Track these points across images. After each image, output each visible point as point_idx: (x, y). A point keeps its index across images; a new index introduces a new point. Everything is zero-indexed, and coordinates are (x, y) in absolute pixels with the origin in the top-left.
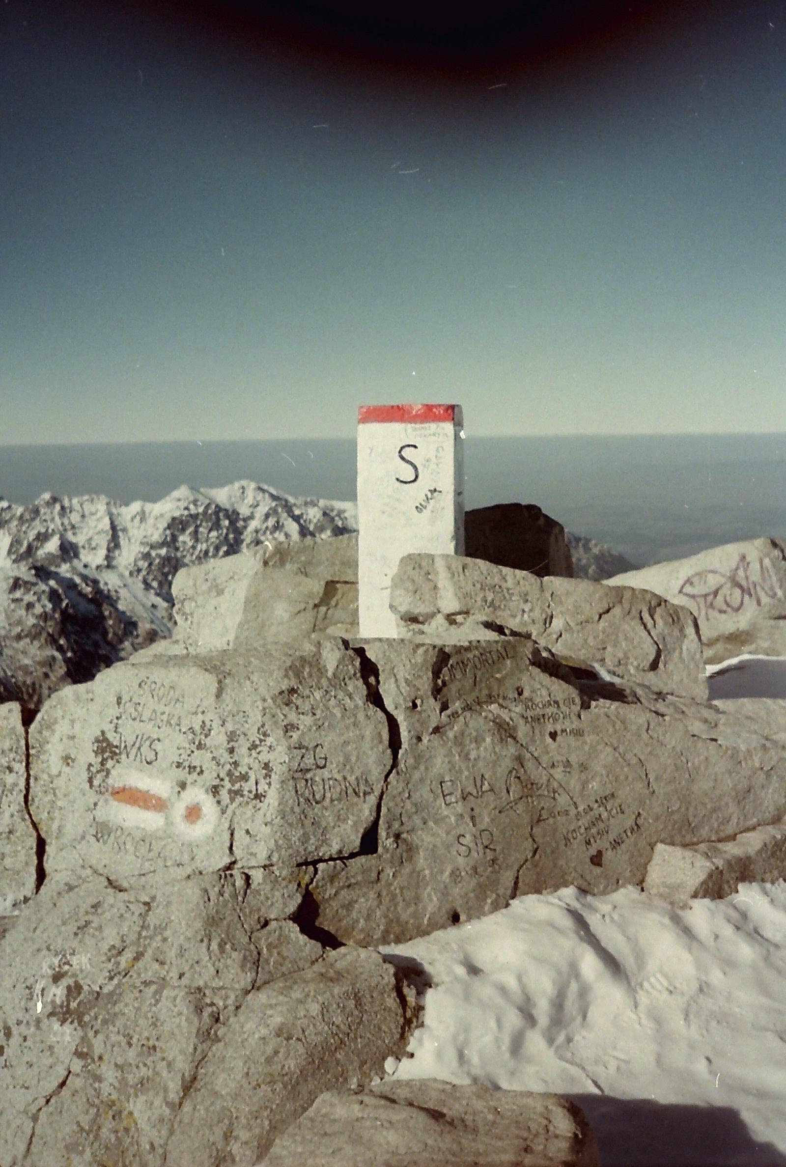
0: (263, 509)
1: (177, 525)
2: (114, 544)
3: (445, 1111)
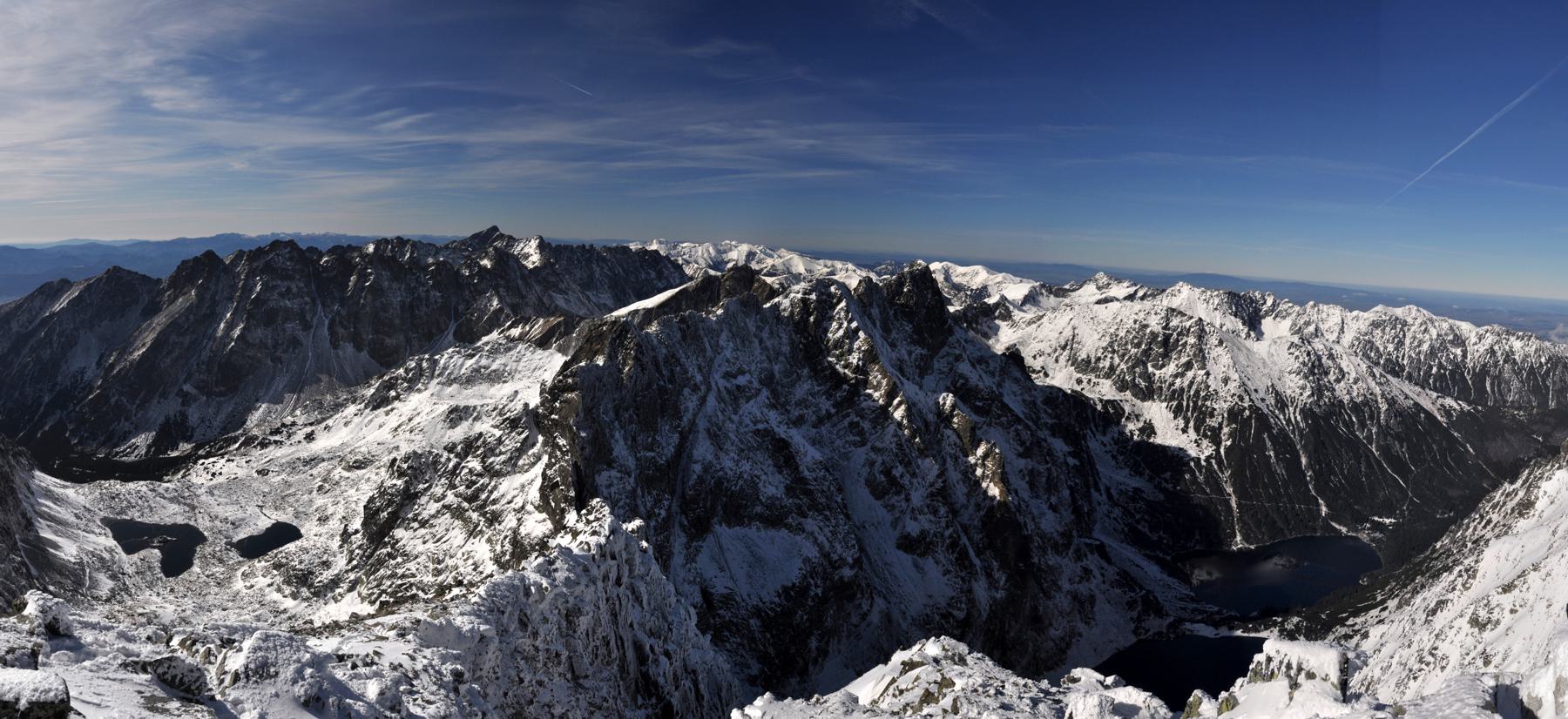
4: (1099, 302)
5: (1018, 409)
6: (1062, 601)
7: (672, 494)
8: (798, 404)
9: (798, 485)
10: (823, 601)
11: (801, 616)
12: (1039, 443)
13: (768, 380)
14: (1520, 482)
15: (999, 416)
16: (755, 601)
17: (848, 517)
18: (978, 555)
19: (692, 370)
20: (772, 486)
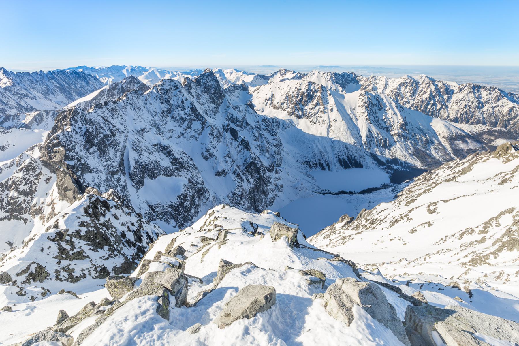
0: (426, 82)
1: (402, 84)
2: (385, 88)
3: (364, 327)
4: (282, 81)
5: (253, 124)
6: (271, 186)
7: (124, 174)
8: (169, 131)
9: (175, 161)
10: (192, 197)
11: (187, 204)
12: (261, 135)
13: (155, 125)
14: (467, 159)
15: (246, 127)
16: (169, 203)
17: (196, 168)
18: (243, 174)
19: (119, 126)
20: (165, 162)
